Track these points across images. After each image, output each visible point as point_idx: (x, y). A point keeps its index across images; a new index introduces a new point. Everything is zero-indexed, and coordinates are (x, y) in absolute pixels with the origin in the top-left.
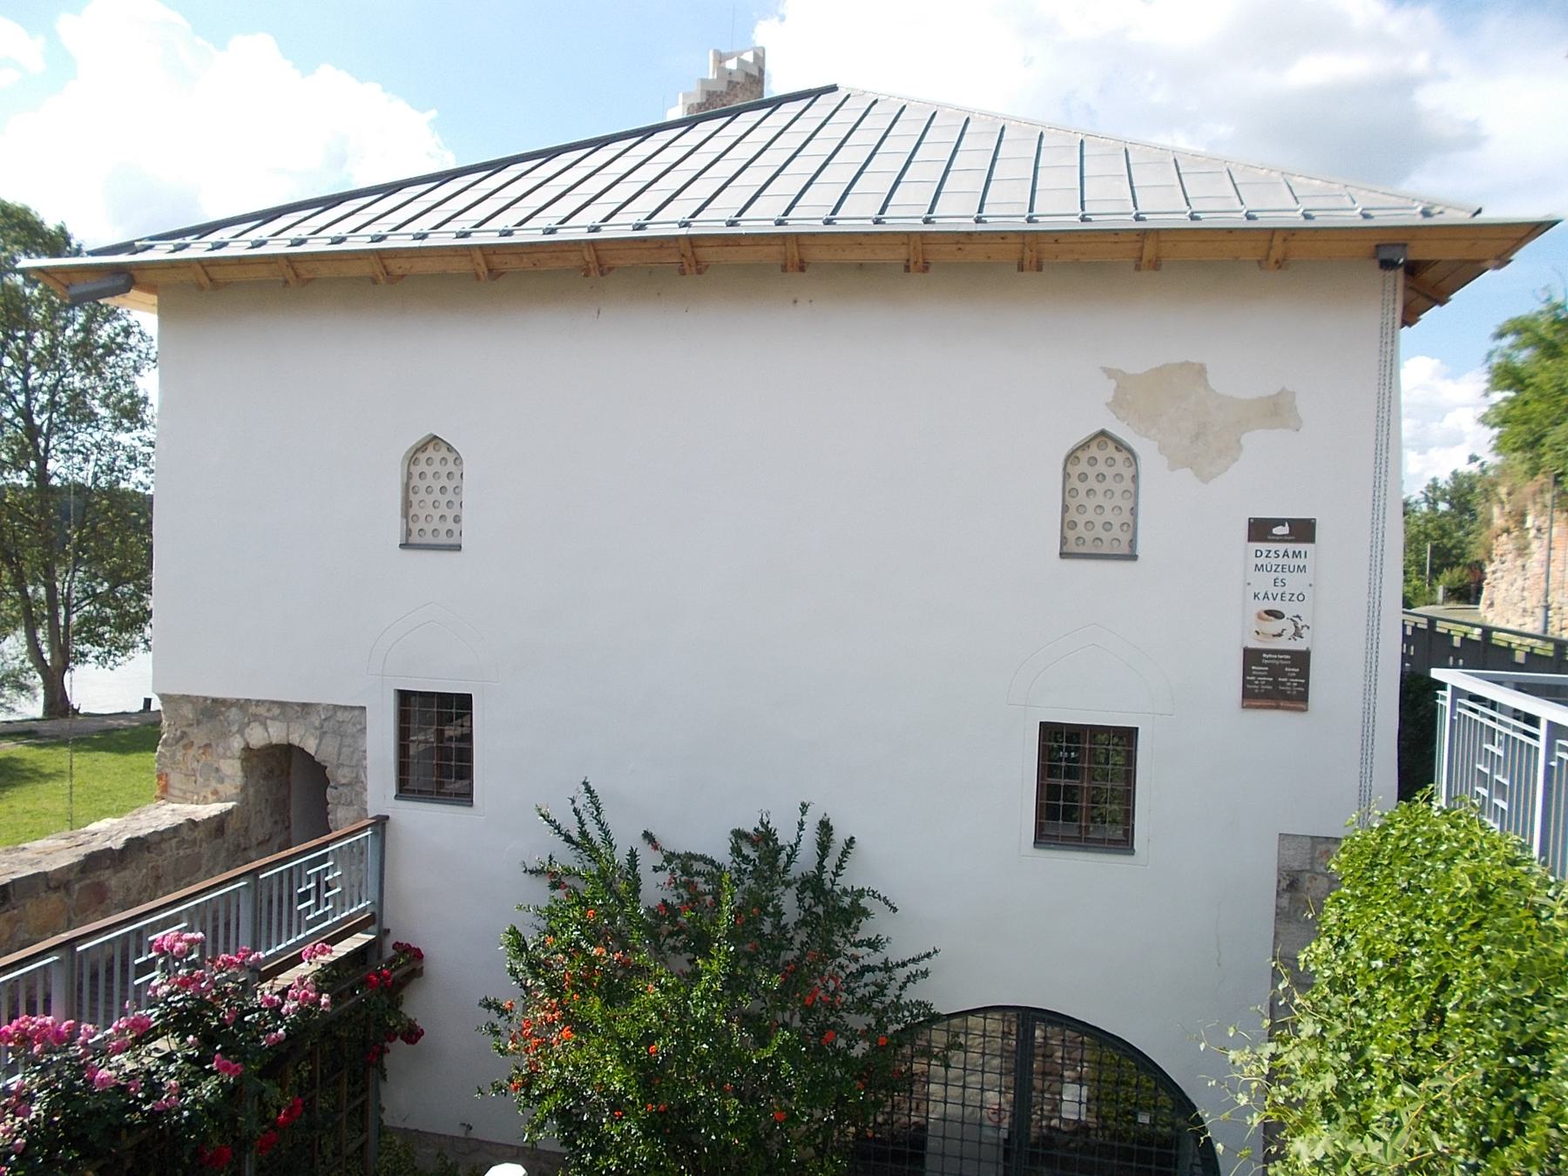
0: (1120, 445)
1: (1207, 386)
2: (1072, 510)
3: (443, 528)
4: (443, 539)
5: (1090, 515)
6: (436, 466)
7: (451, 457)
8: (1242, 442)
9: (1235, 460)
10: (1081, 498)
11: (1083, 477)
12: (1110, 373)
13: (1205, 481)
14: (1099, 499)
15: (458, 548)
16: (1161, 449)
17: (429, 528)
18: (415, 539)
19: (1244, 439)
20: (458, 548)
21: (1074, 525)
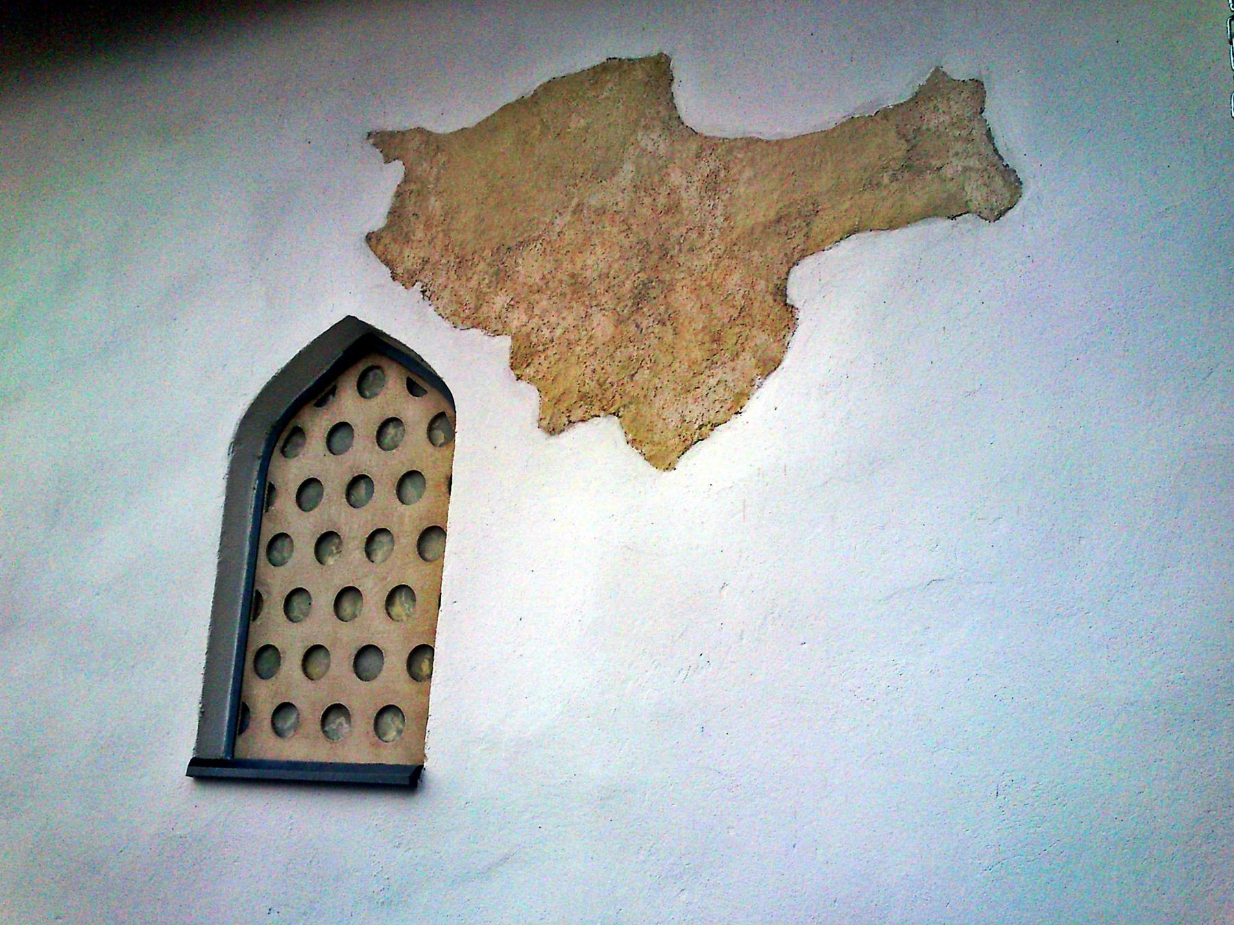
0: (421, 378)
1: (673, 123)
2: (273, 608)
3: (362, 698)
4: (355, 747)
5: (319, 624)
6: (363, 454)
7: (416, 412)
8: (795, 294)
9: (770, 365)
10: (296, 568)
11: (309, 490)
12: (387, 144)
13: (663, 460)
14: (347, 565)
15: (407, 780)
16: (521, 361)
17: (309, 697)
18: (263, 744)
19: (802, 284)
20: (407, 780)
21: (268, 659)
